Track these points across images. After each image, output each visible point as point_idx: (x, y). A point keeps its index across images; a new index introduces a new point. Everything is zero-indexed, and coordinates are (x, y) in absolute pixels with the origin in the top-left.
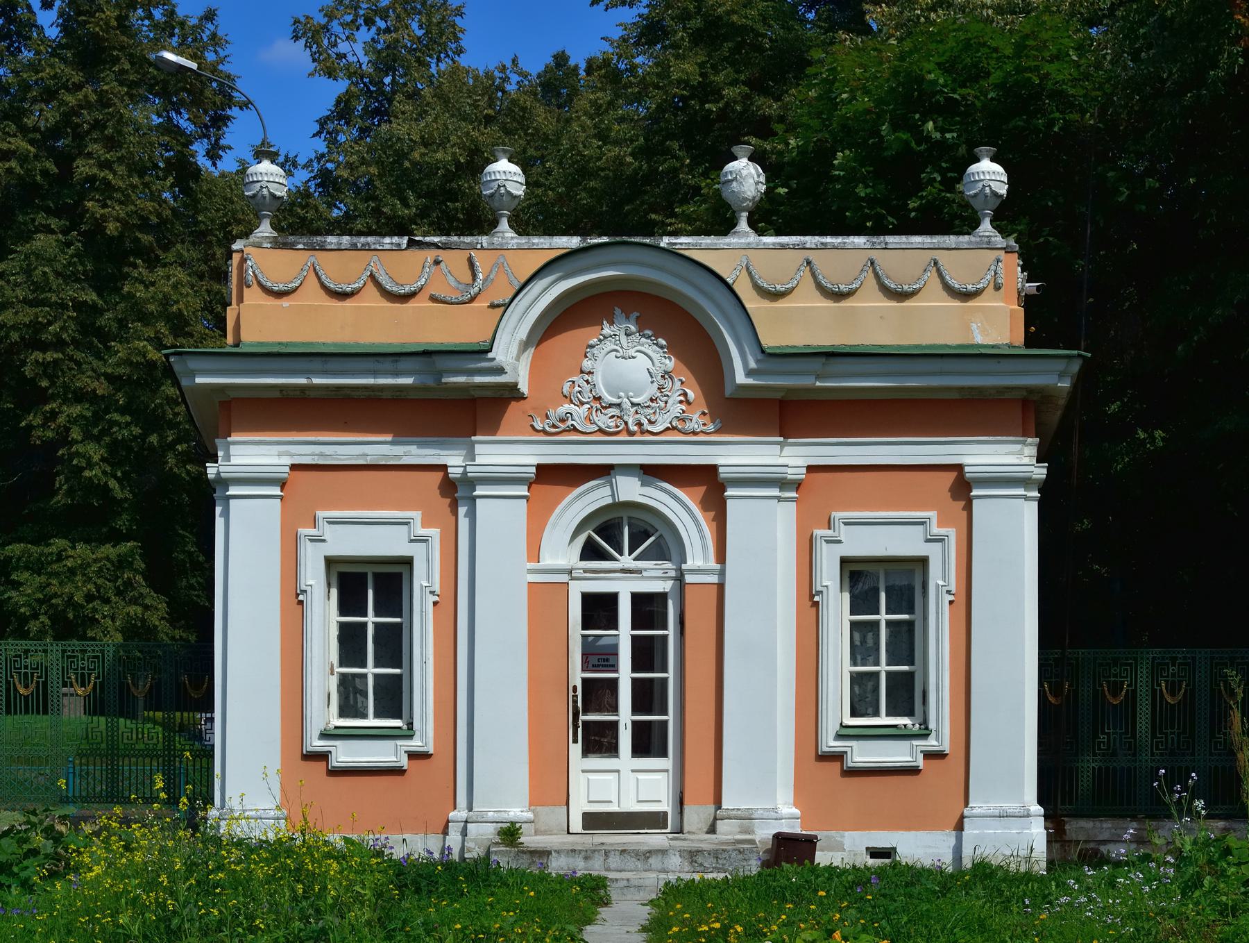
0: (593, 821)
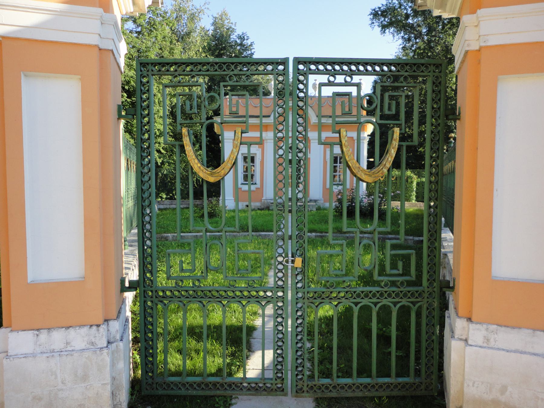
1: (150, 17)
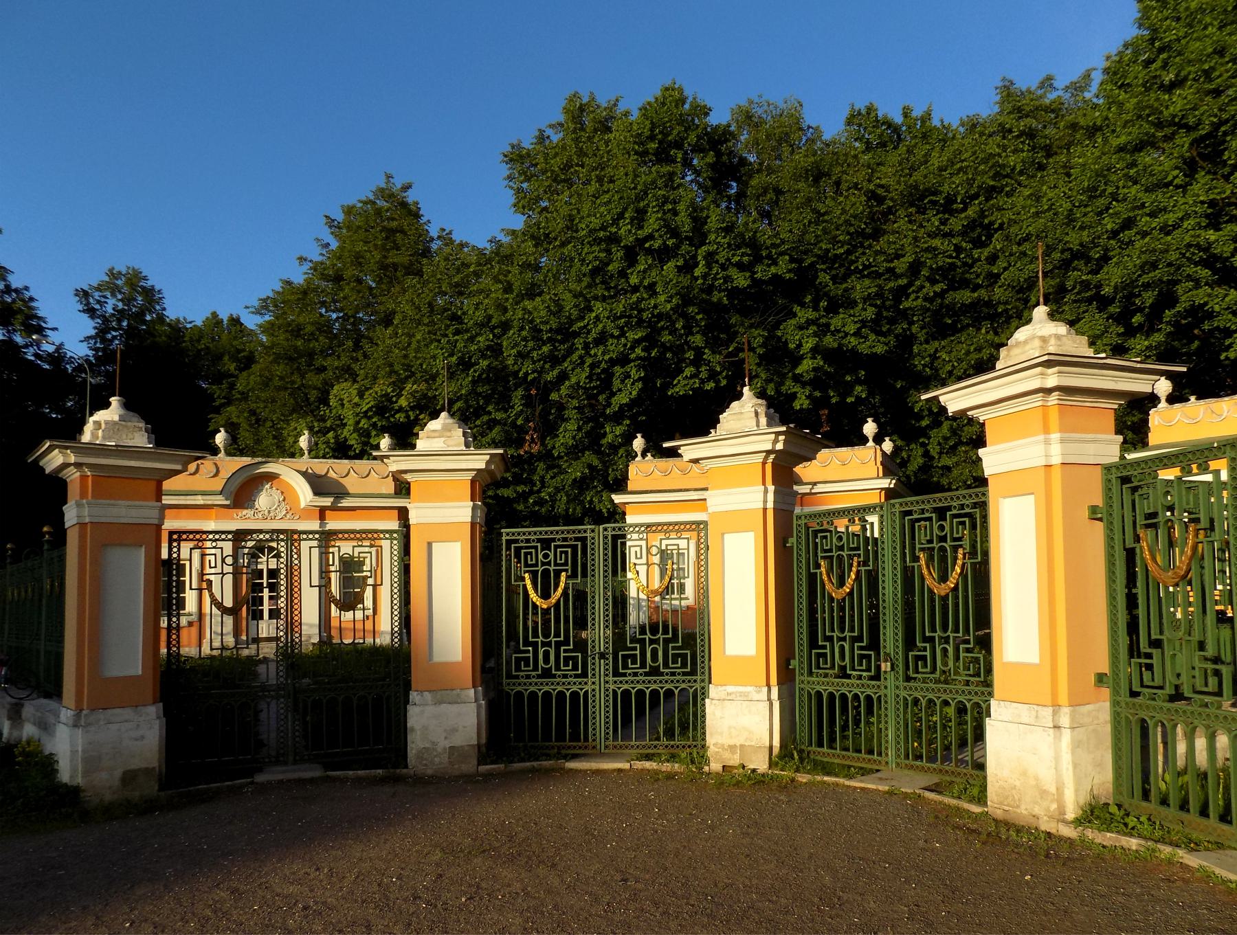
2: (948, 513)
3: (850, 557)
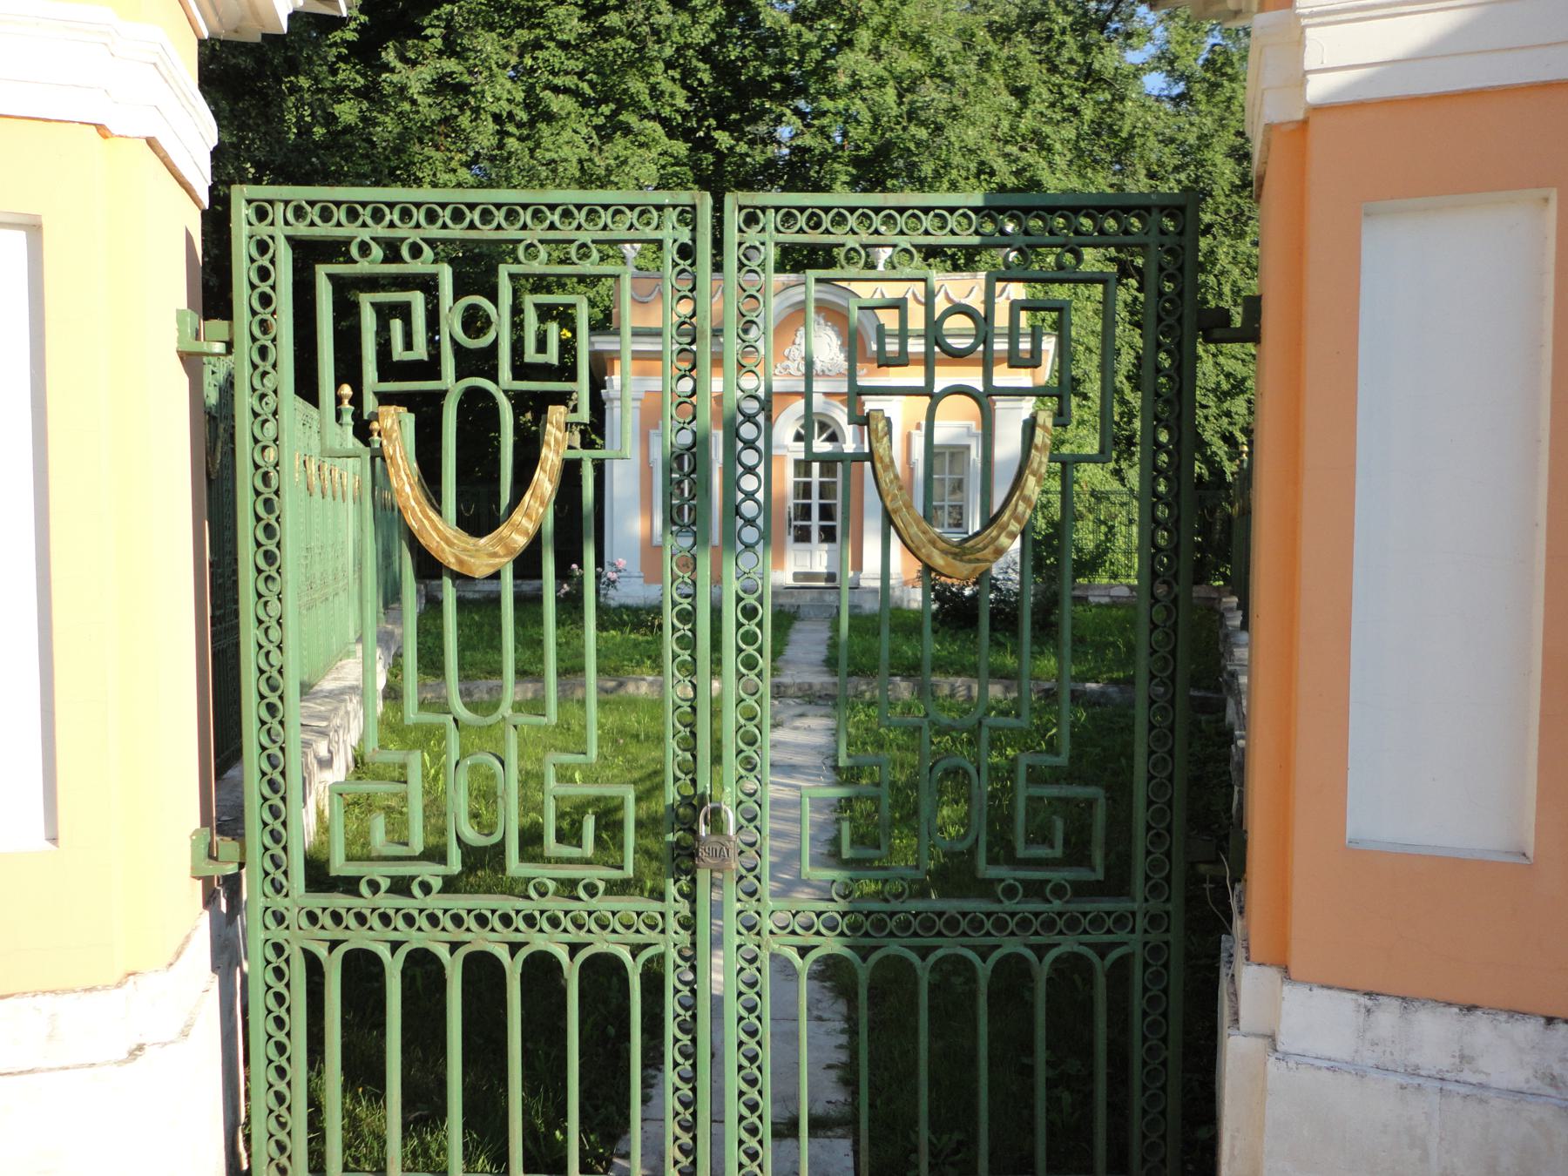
0: (796, 576)
1: (1214, 45)
2: (504, 271)
3: (533, 406)
